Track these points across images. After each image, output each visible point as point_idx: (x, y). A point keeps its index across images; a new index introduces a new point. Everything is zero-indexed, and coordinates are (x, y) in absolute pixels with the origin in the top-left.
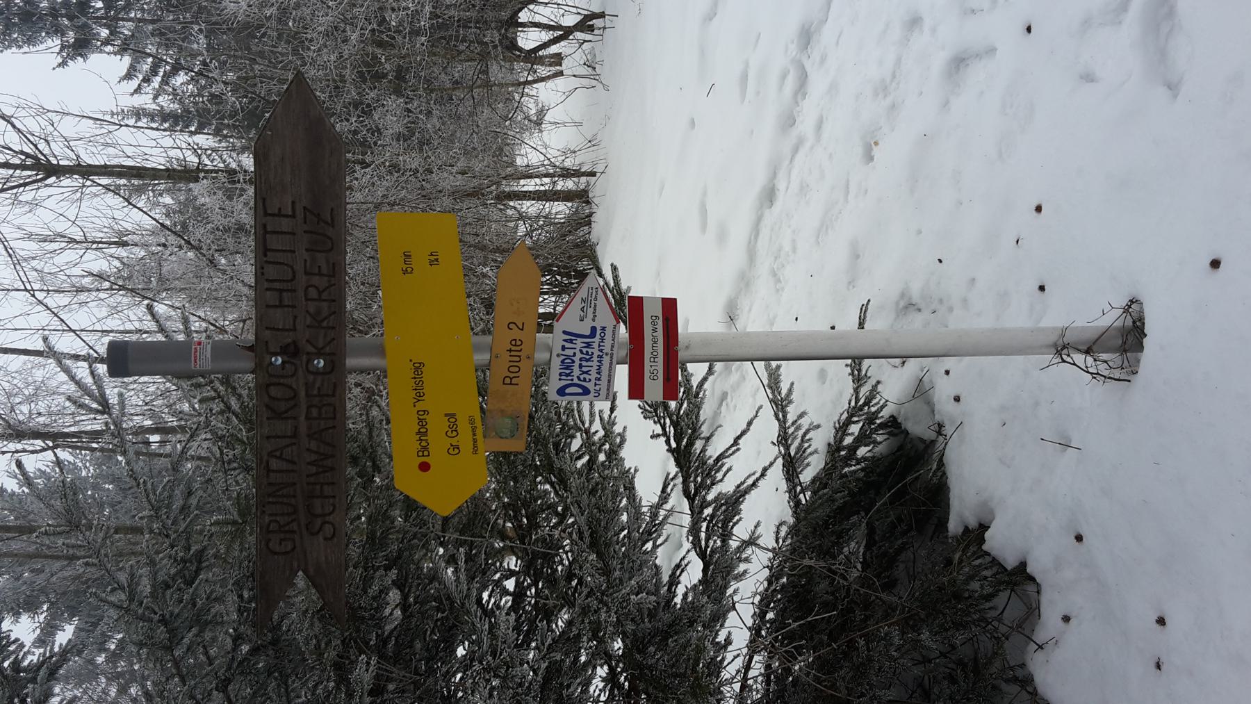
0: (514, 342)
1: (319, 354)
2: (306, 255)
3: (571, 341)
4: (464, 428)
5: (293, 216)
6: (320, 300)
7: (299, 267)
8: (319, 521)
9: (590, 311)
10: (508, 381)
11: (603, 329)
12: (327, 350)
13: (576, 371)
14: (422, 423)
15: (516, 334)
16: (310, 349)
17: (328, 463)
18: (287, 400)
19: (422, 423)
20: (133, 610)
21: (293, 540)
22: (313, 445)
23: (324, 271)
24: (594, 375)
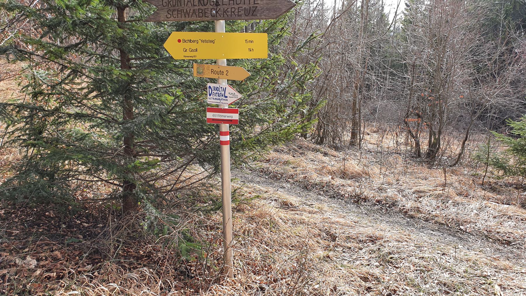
0: (223, 72)
1: (217, 12)
2: (244, 7)
3: (223, 90)
4: (193, 54)
5: (254, 4)
6: (231, 12)
7: (240, 5)
8: (171, 13)
9: (232, 96)
10: (212, 71)
11: (227, 100)
12: (218, 15)
13: (215, 92)
14: (194, 41)
15: (225, 73)
16: (218, 9)
17: (187, 16)
18: (204, 3)
19: (194, 41)
20: (486, 182)
21: (166, 6)
22: (191, 11)
23: (240, 13)
24: (214, 97)
